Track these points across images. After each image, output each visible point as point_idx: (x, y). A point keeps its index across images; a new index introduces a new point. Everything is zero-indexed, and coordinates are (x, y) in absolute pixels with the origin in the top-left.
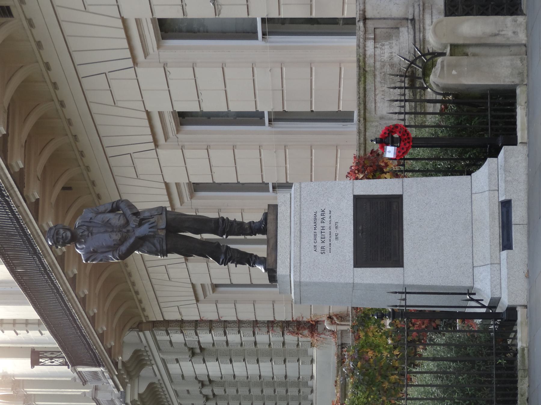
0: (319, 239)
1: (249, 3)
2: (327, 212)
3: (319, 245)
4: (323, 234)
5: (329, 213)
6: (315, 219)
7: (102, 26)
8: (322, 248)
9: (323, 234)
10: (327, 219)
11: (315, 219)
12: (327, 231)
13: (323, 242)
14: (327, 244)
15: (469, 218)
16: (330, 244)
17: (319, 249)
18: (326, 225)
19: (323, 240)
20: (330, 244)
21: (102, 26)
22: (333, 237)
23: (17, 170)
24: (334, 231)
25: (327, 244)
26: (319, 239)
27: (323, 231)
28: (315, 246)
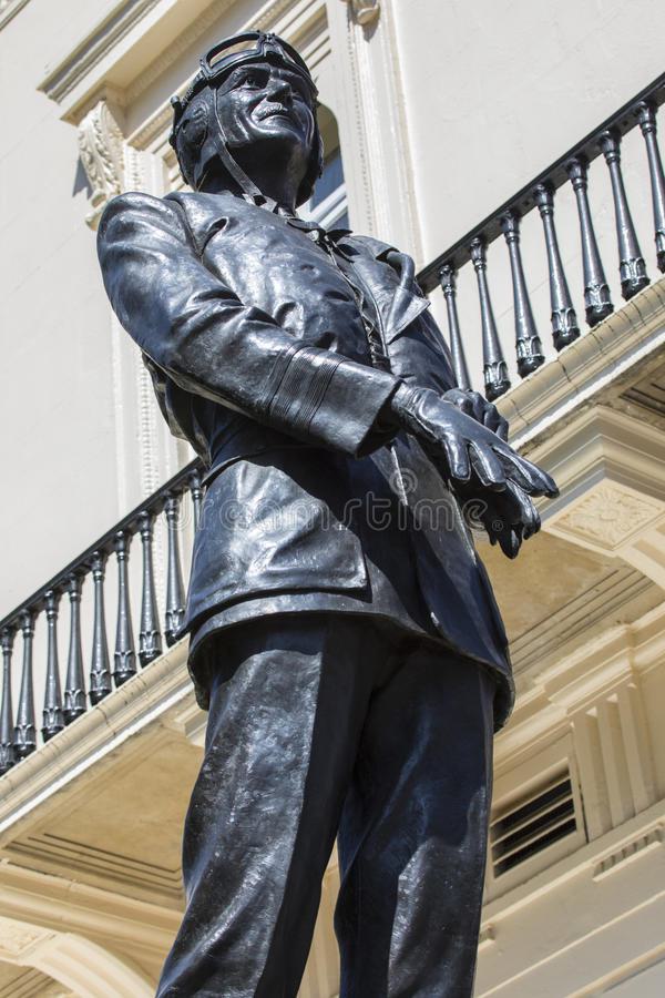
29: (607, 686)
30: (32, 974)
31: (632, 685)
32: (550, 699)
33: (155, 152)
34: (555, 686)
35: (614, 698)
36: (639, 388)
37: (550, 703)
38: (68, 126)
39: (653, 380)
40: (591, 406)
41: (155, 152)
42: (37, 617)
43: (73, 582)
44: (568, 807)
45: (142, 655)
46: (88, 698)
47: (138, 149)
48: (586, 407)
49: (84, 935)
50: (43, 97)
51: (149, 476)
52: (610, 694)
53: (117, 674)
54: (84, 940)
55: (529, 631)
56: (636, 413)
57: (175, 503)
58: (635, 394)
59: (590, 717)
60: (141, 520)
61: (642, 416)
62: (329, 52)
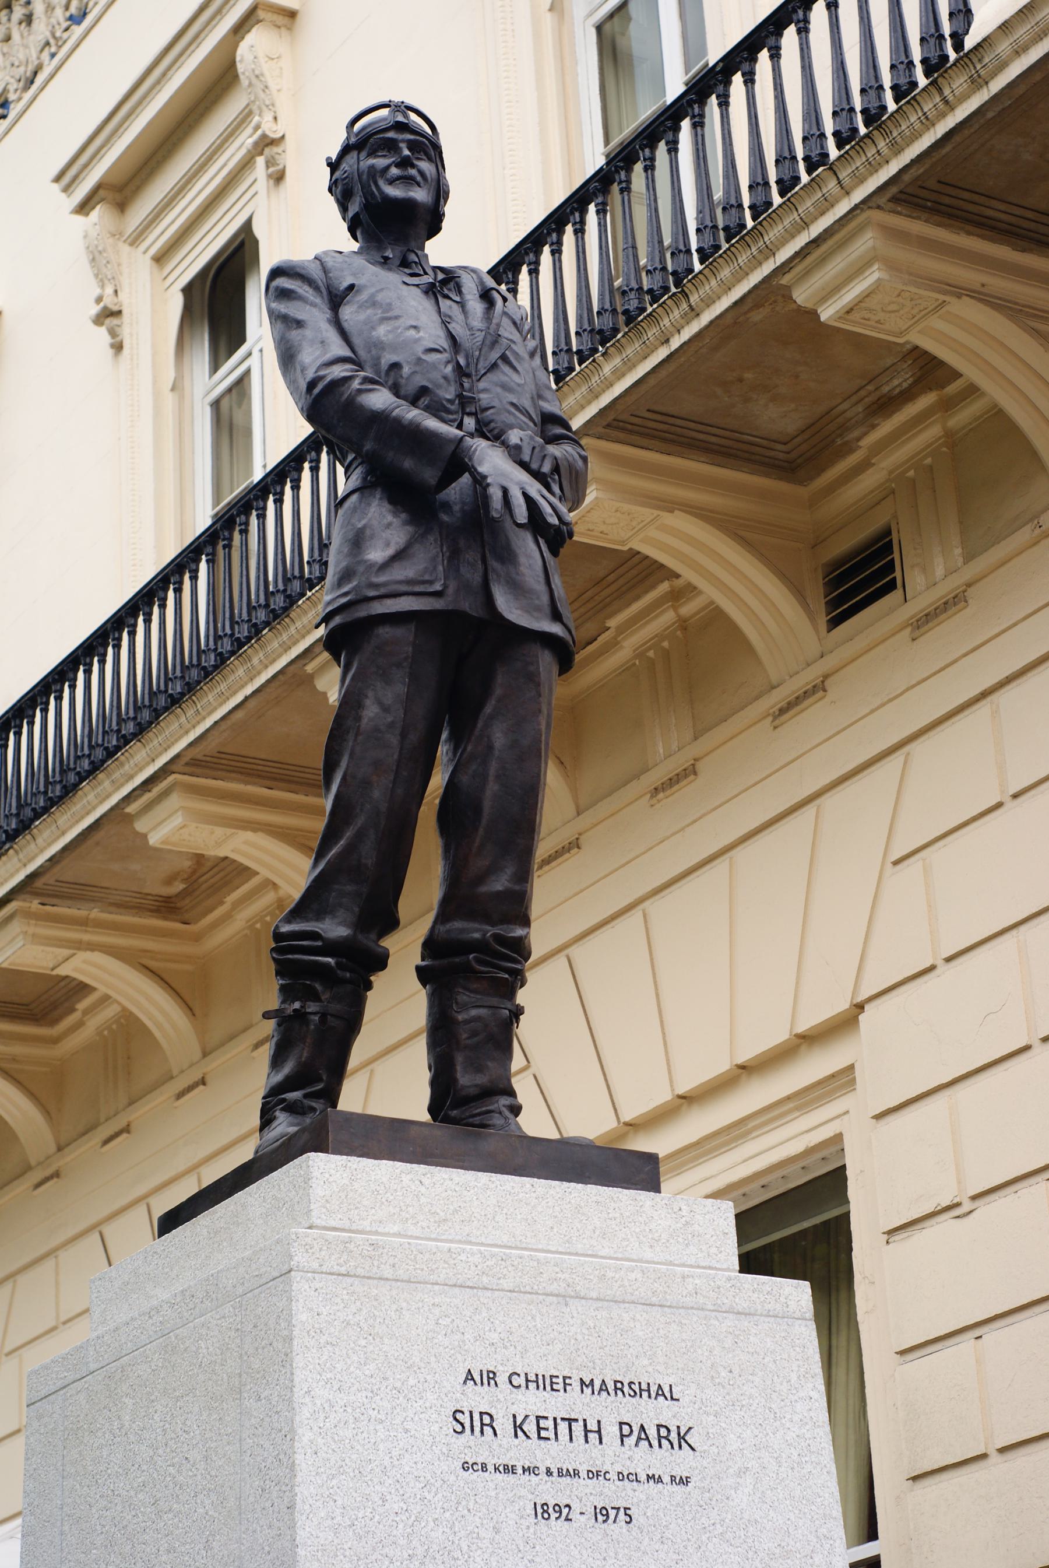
0: (532, 1402)
1: (1010, 804)
2: (680, 1462)
3: (505, 1403)
4: (563, 1427)
5: (678, 1472)
6: (638, 1391)
7: (664, 1034)
8: (486, 1422)
9: (563, 1427)
10: (643, 1459)
11: (638, 1391)
12: (577, 1454)
13: (518, 1428)
14: (506, 1447)
15: (834, 1337)
16: (509, 1469)
17: (477, 1399)
18: (612, 1454)
19: (530, 1427)
20: (509, 1469)
21: (664, 1034)
22: (552, 1491)
23: (802, 296)
24: (583, 1495)
25: (506, 1447)
26: (532, 1402)
27: (578, 1428)
28: (491, 1376)
29: (922, 450)
30: (226, 862)
31: (944, 449)
32: (873, 461)
33: (145, 252)
34: (622, 629)
35: (928, 461)
36: (620, 418)
37: (874, 464)
38: (79, 219)
39: (920, 183)
40: (862, 210)
41: (145, 252)
42: (656, 147)
43: (696, 106)
44: (890, 567)
45: (726, 229)
46: (722, 234)
47: (132, 244)
48: (858, 211)
49: (696, 515)
50: (56, 187)
51: (134, 565)
52: (266, 916)
53: (579, 352)
54: (688, 516)
55: (845, 400)
56: (908, 213)
57: (805, 15)
58: (903, 197)
59: (649, 658)
60: (690, 103)
61: (915, 215)
62: (256, 193)
